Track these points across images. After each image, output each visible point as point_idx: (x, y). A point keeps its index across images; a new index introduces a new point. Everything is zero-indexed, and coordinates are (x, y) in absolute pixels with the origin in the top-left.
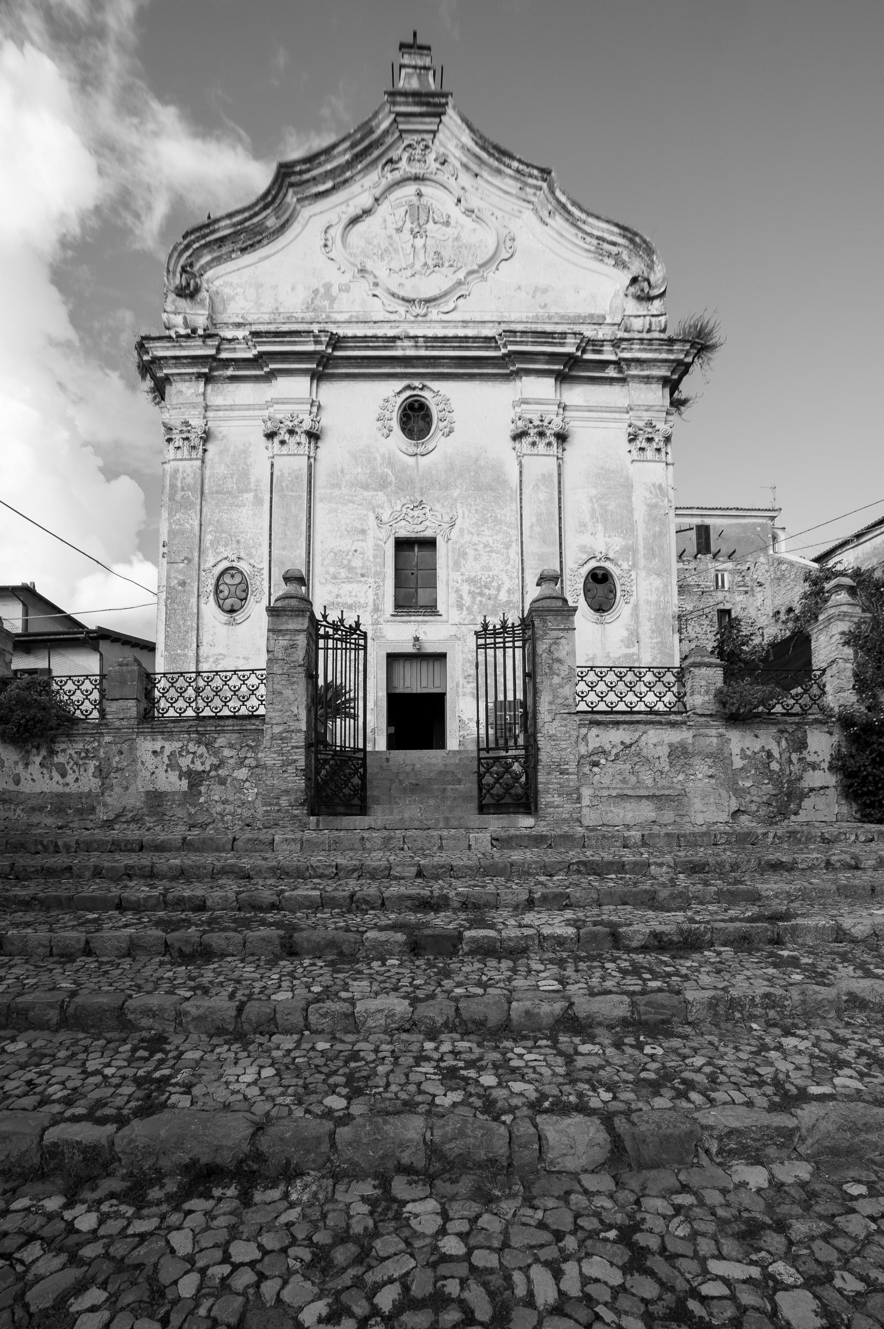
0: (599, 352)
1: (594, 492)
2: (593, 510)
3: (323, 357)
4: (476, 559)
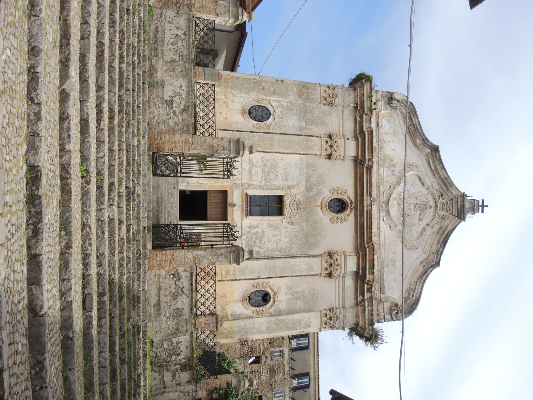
0: (367, 291)
1: (306, 293)
2: (298, 293)
3: (363, 162)
4: (273, 235)
